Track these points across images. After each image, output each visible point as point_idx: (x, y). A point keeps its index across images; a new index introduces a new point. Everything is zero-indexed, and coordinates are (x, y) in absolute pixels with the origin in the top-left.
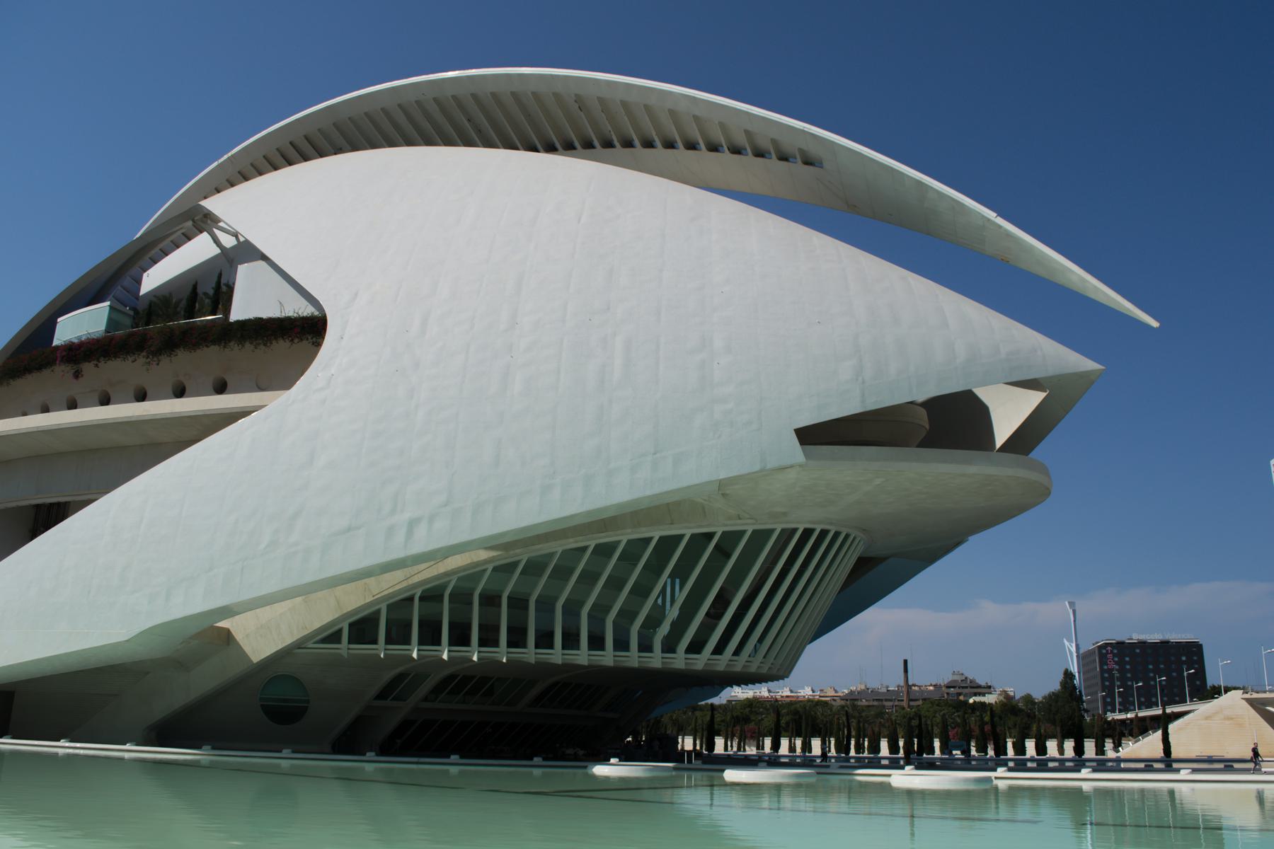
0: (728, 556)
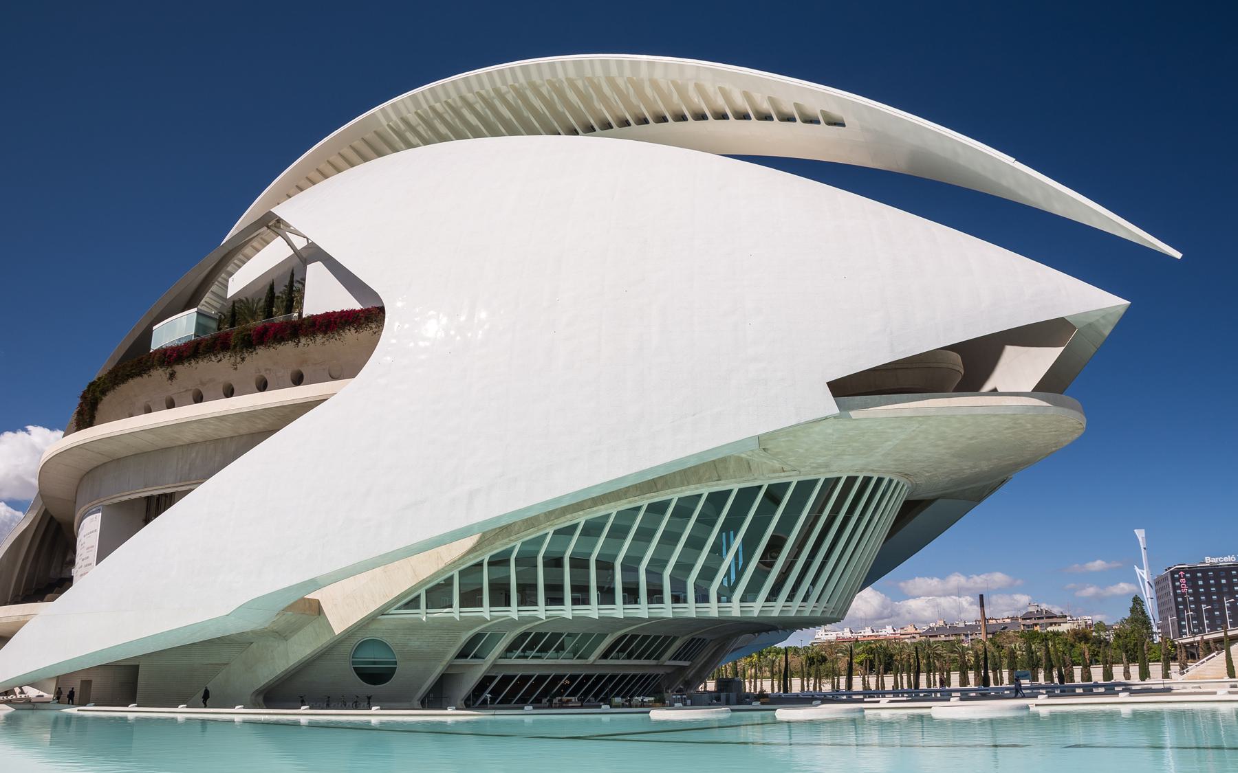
0: (777, 502)
